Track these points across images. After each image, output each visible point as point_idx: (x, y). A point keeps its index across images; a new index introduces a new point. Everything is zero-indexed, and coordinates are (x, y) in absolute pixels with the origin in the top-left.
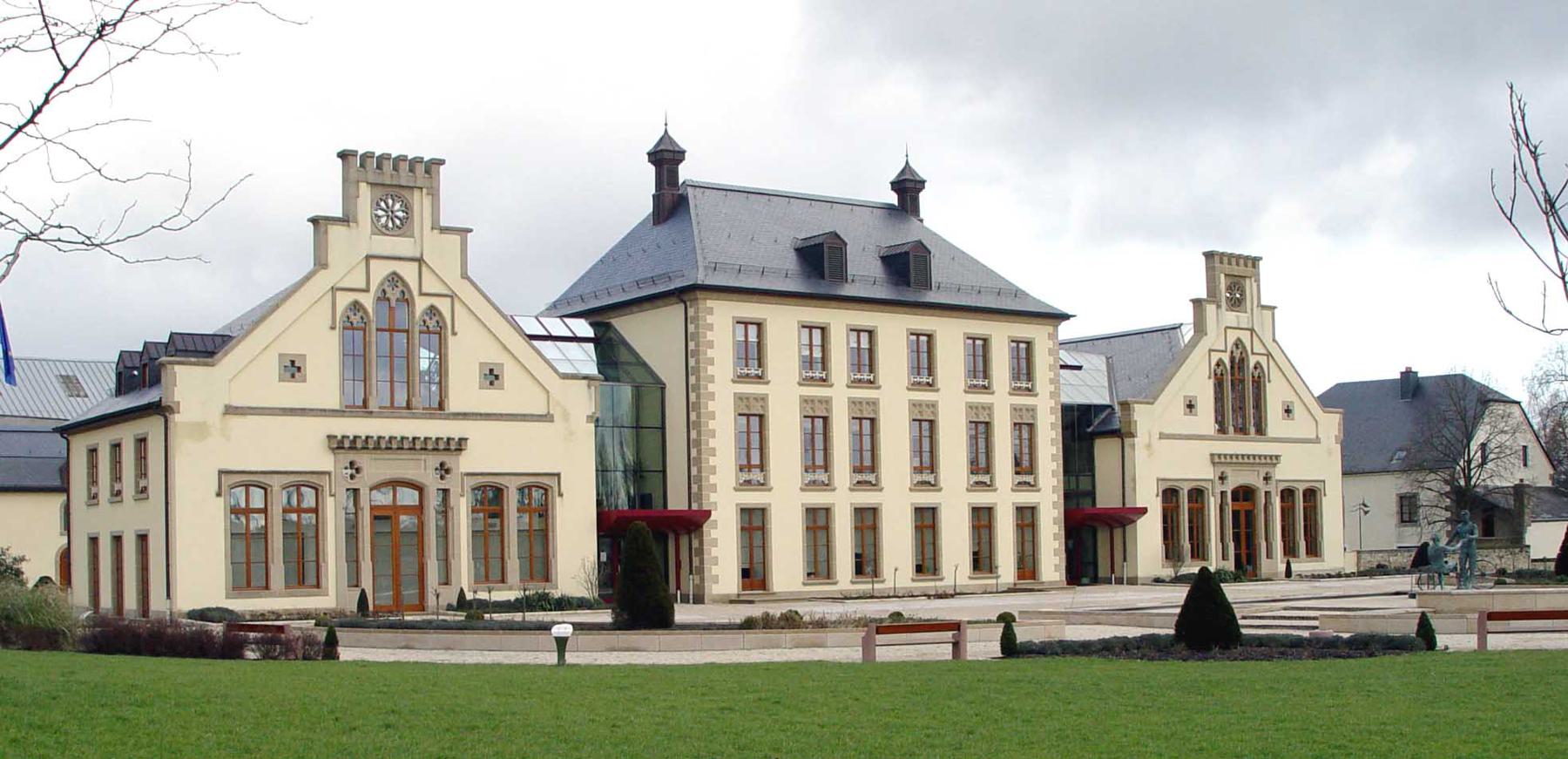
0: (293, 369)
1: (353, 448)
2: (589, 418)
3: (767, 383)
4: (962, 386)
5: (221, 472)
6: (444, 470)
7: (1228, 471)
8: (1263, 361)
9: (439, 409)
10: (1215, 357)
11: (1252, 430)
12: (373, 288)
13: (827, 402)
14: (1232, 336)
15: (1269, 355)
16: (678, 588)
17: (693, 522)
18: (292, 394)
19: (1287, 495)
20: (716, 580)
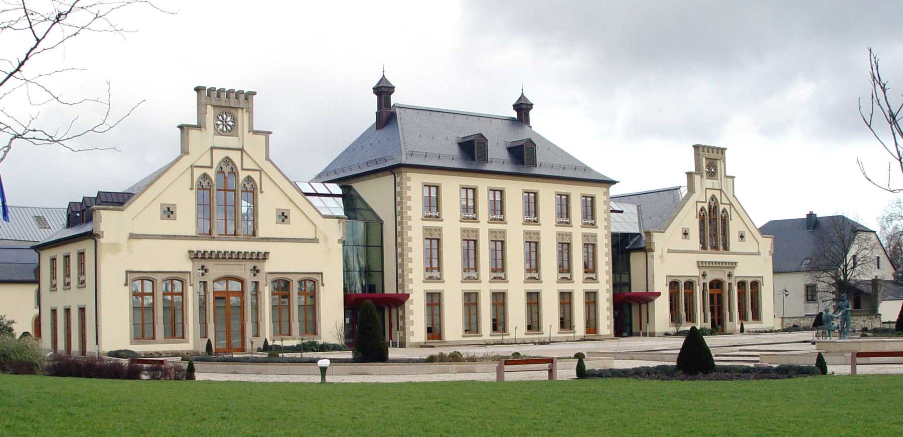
0: (169, 212)
1: (203, 258)
2: (339, 241)
3: (442, 220)
4: (554, 223)
5: (127, 272)
6: (256, 271)
7: (707, 271)
8: (727, 208)
9: (253, 235)
10: (700, 206)
11: (721, 247)
12: (215, 166)
13: (476, 231)
14: (710, 194)
15: (731, 204)
16: (391, 338)
17: (399, 301)
18: (168, 227)
19: (741, 285)
20: (412, 334)
